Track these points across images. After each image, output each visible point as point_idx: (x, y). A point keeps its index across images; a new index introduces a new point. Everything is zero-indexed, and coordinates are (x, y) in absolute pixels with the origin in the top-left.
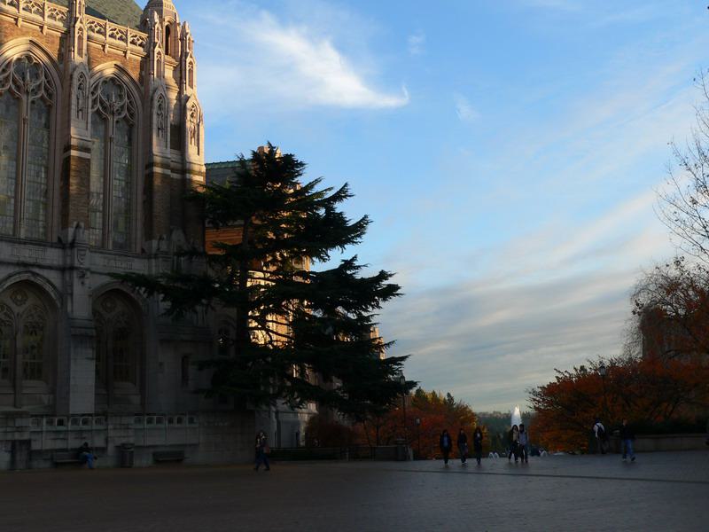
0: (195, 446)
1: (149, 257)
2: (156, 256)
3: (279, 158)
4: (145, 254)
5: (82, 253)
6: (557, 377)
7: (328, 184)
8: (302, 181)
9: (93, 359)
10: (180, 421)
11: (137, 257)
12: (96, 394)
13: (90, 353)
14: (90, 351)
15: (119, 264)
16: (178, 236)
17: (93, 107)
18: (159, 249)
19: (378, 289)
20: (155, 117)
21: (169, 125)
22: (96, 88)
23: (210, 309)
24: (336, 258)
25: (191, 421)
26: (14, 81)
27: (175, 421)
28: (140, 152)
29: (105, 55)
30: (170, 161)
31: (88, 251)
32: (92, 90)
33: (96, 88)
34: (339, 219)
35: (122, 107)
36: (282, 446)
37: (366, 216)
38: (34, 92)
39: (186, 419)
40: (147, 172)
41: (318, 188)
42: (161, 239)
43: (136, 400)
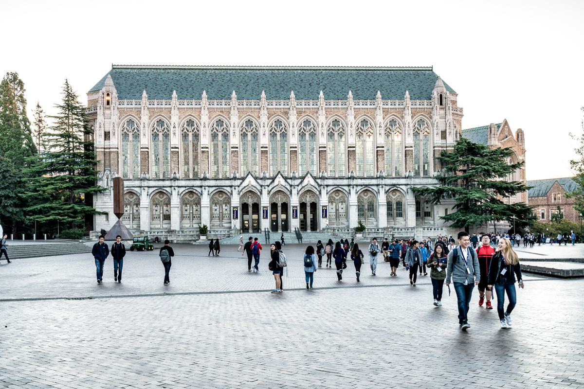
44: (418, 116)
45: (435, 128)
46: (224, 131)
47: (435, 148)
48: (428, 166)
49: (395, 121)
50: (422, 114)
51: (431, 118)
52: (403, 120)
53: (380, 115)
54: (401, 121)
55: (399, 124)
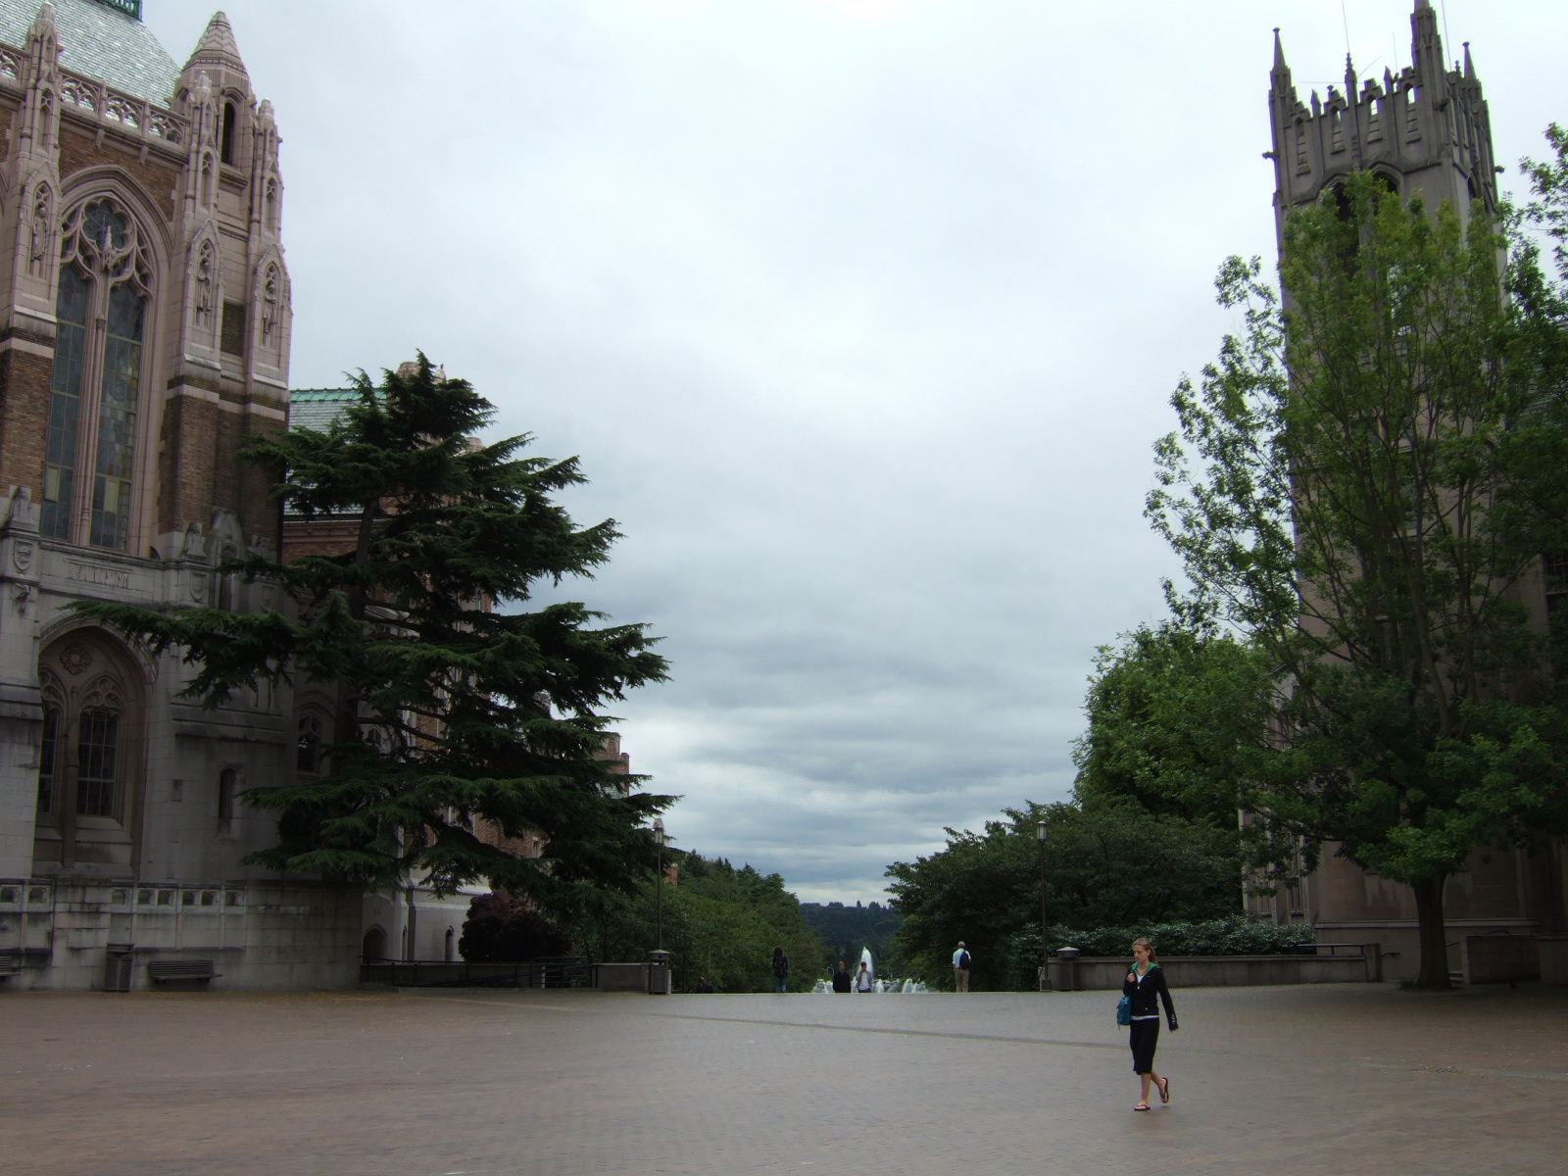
0: (234, 953)
1: (165, 566)
2: (178, 566)
3: (441, 385)
4: (155, 561)
5: (25, 549)
6: (950, 843)
7: (543, 448)
8: (484, 437)
9: (33, 768)
10: (207, 900)
11: (140, 563)
12: (36, 839)
13: (30, 754)
14: (31, 751)
15: (100, 577)
16: (225, 526)
17: (63, 255)
18: (185, 552)
19: (624, 659)
20: (192, 284)
21: (221, 304)
22: (72, 217)
23: (282, 680)
24: (545, 592)
25: (232, 901)
26: (83, 247)
27: (198, 899)
28: (158, 355)
29: (96, 150)
30: (217, 375)
31: (36, 547)
32: (63, 219)
33: (72, 217)
34: (554, 520)
35: (125, 260)
36: (417, 957)
37: (611, 522)
38: (118, 269)
39: (220, 897)
40: (171, 394)
41: (517, 455)
42: (191, 530)
43: (123, 855)
44: (91, 177)
45: (194, 271)
46: (125, 277)
47: (188, 390)
48: (125, 489)
49: (122, 219)
50: (123, 170)
51: (169, 214)
52: (171, 225)
53: (44, 144)
54: (161, 224)
55: (140, 242)
